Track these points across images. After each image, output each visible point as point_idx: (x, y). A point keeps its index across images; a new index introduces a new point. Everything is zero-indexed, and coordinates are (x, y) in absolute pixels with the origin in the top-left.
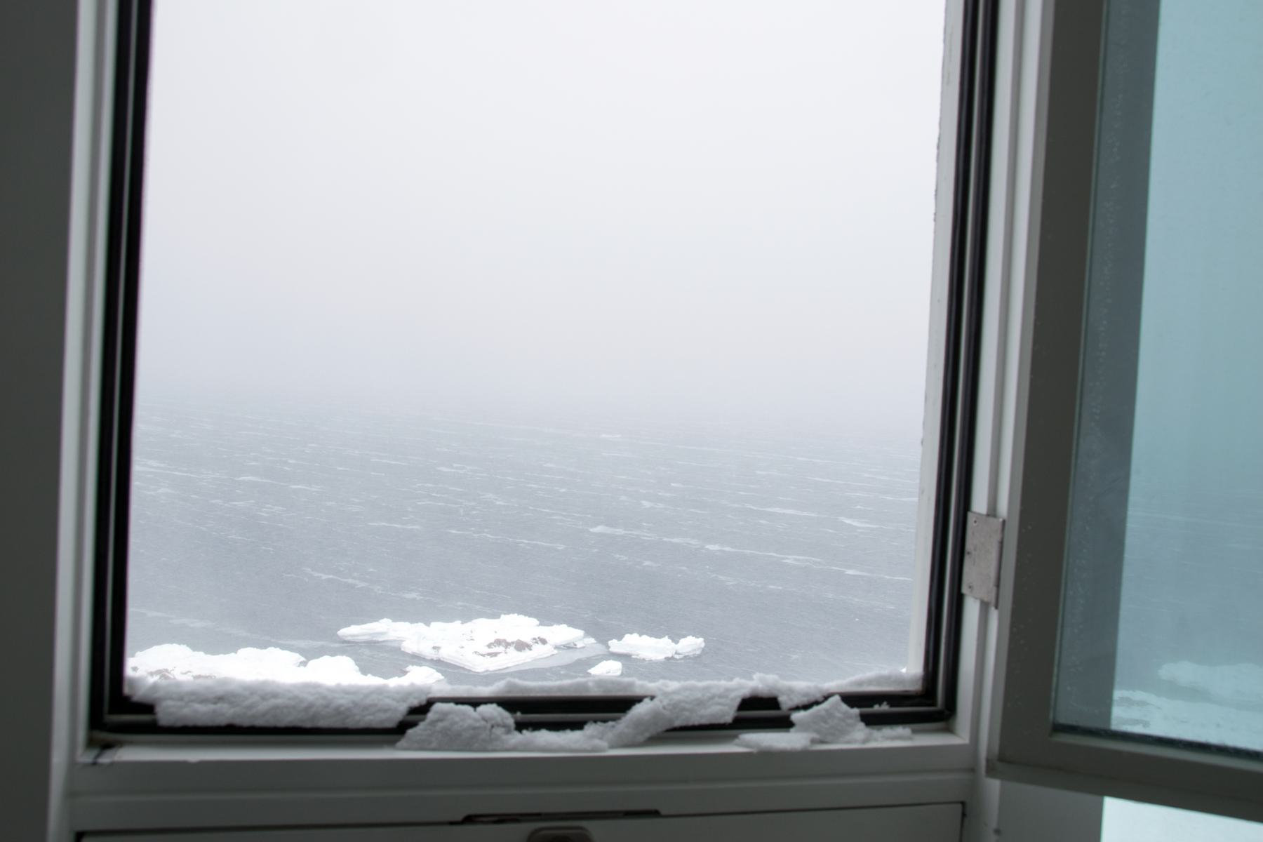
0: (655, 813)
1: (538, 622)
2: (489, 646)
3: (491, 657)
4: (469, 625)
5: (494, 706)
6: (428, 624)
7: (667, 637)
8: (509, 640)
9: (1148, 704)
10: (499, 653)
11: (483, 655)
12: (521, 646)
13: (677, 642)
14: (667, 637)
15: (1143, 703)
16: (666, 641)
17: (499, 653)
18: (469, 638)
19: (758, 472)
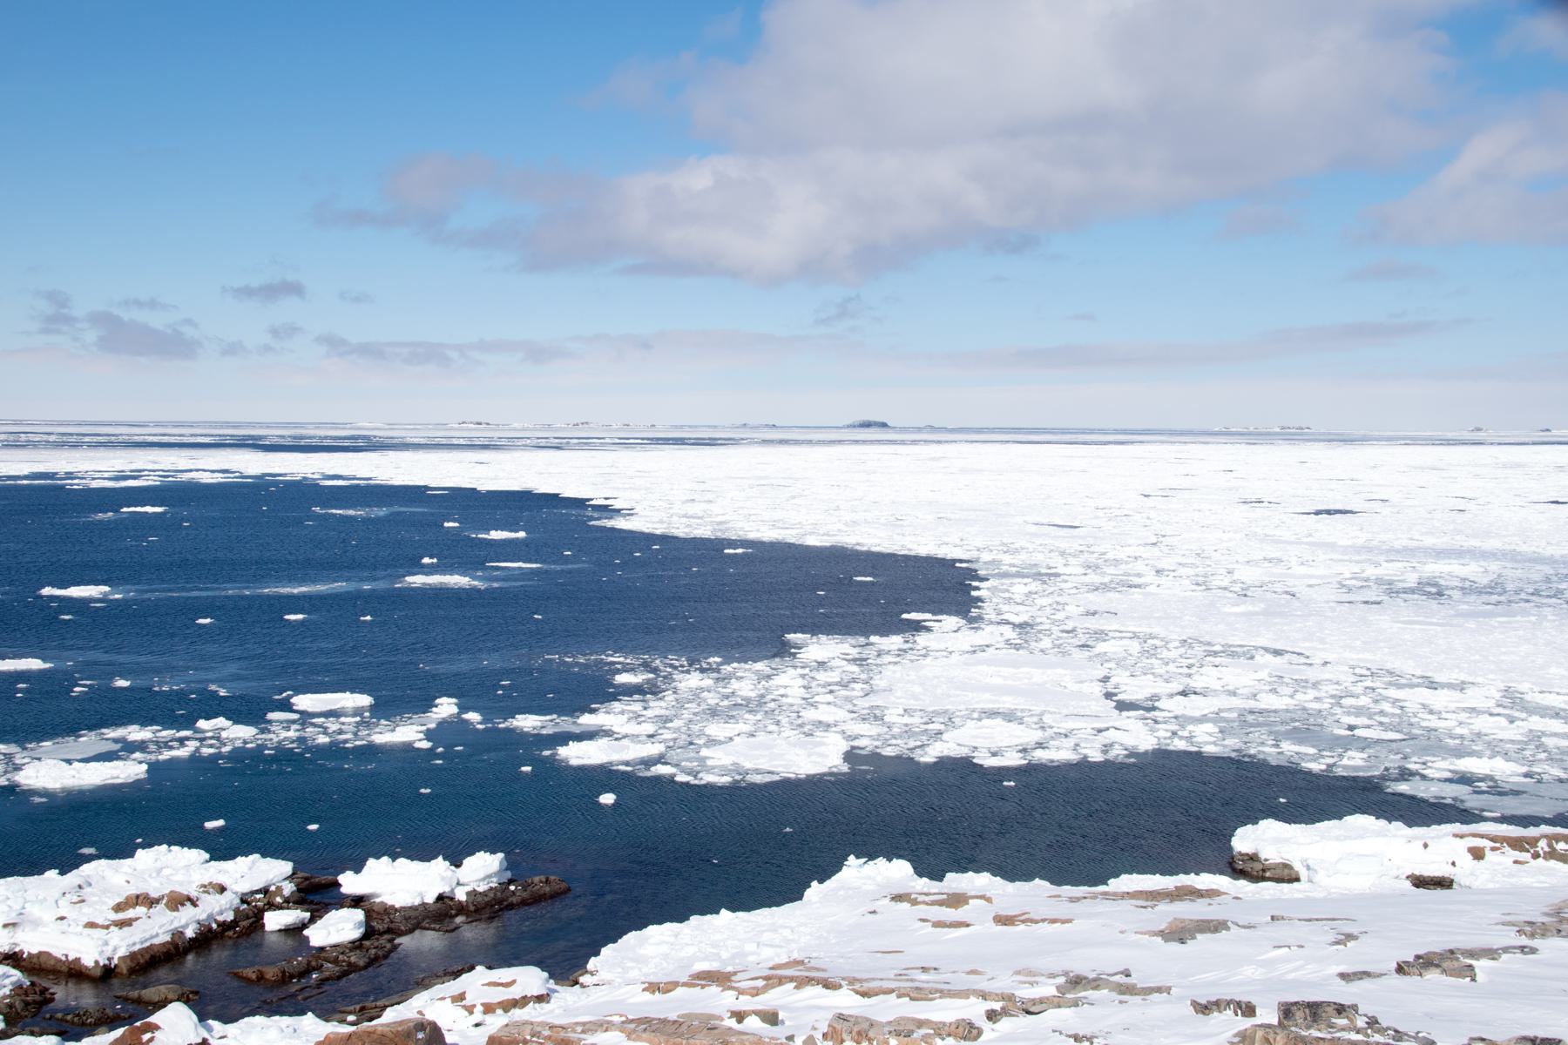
0: (1366, 974)
1: (207, 856)
2: (118, 908)
3: (1286, 866)
4: (74, 877)
5: (761, 980)
6: (1197, 874)
7: (440, 858)
8: (154, 895)
9: (1161, 933)
10: (137, 919)
11: (107, 927)
12: (178, 901)
13: (458, 865)
14: (440, 858)
15: (1211, 894)
16: (440, 865)
17: (137, 919)
18: (75, 899)
19: (266, 752)
